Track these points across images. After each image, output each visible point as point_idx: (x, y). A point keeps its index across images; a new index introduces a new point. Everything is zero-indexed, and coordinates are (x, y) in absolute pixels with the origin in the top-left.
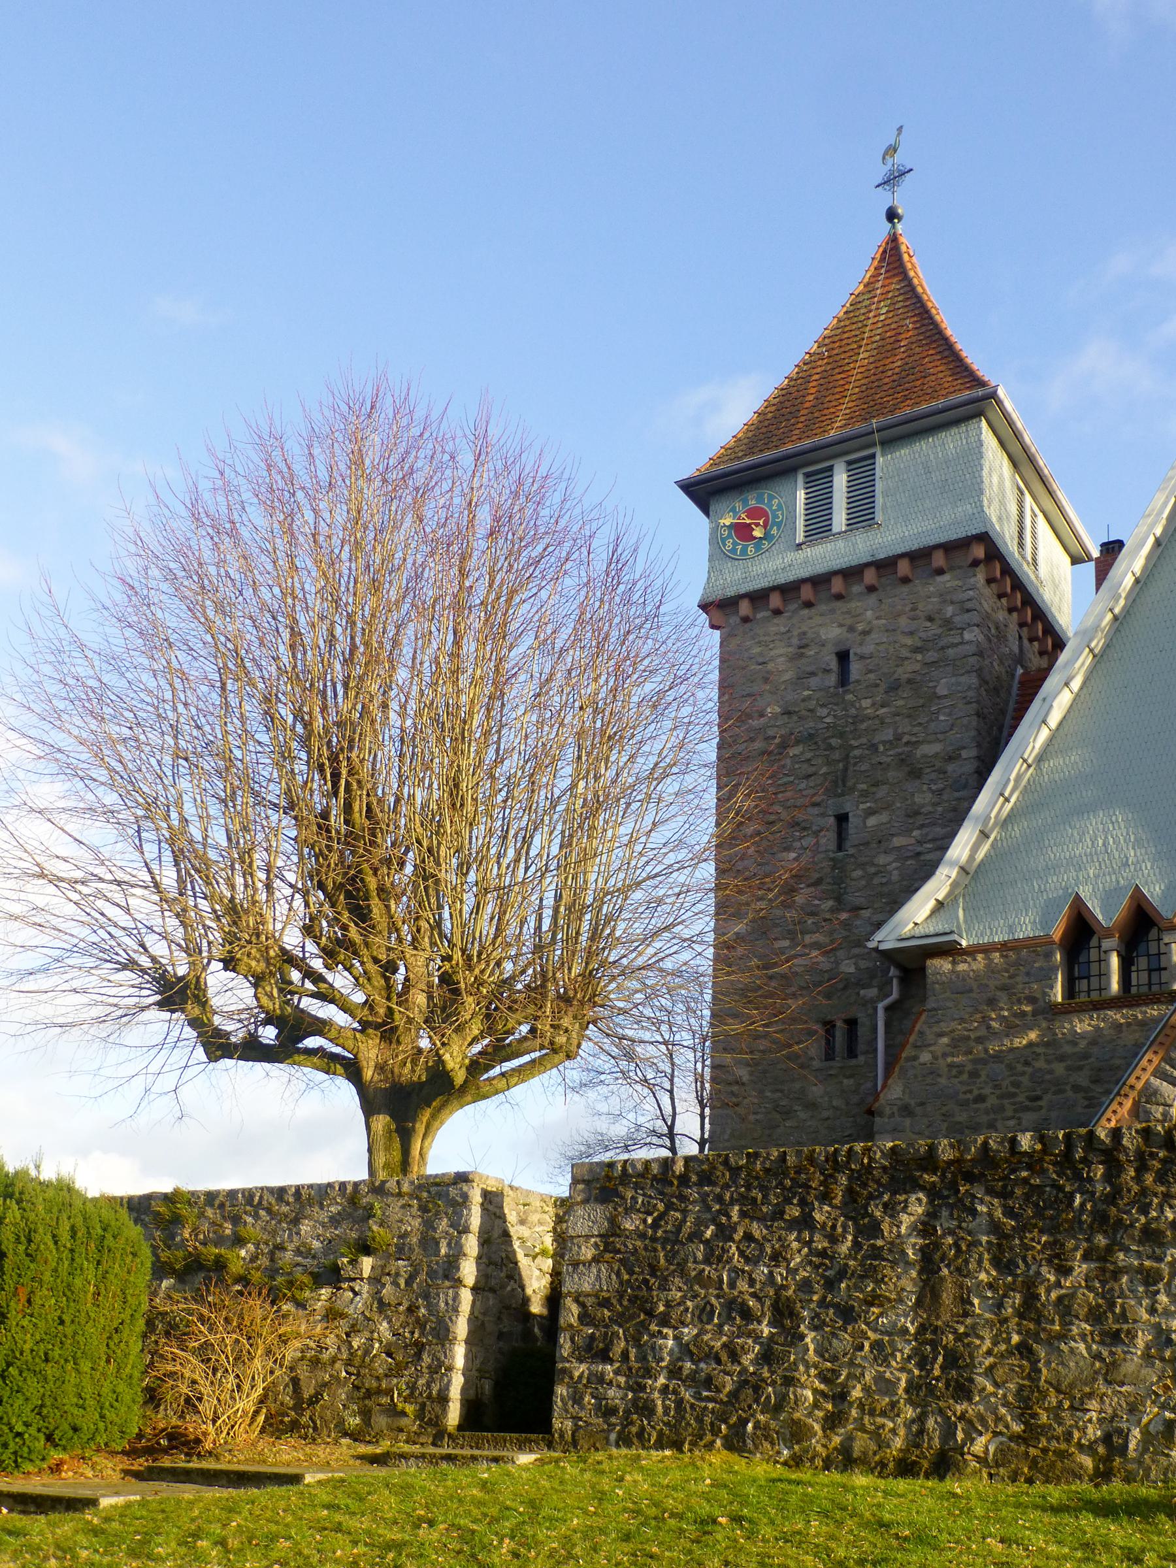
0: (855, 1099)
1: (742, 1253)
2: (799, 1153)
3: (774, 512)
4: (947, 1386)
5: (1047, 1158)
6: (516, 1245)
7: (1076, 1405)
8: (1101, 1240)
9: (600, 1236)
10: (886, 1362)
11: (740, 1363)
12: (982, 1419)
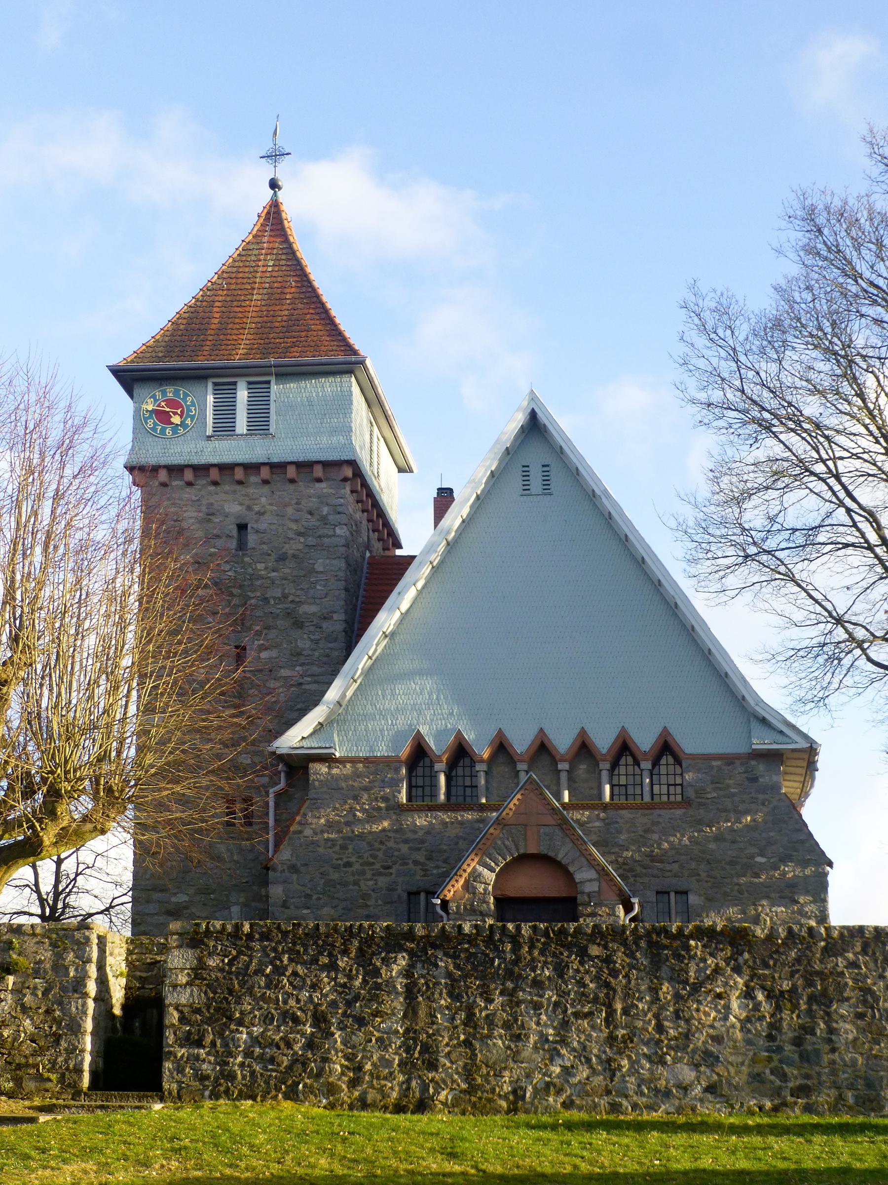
0: (251, 856)
1: (291, 984)
2: (327, 925)
3: (188, 406)
4: (423, 1063)
5: (479, 938)
6: (108, 969)
7: (497, 1073)
8: (510, 985)
9: (191, 969)
10: (386, 1049)
11: (292, 1049)
12: (444, 1082)
